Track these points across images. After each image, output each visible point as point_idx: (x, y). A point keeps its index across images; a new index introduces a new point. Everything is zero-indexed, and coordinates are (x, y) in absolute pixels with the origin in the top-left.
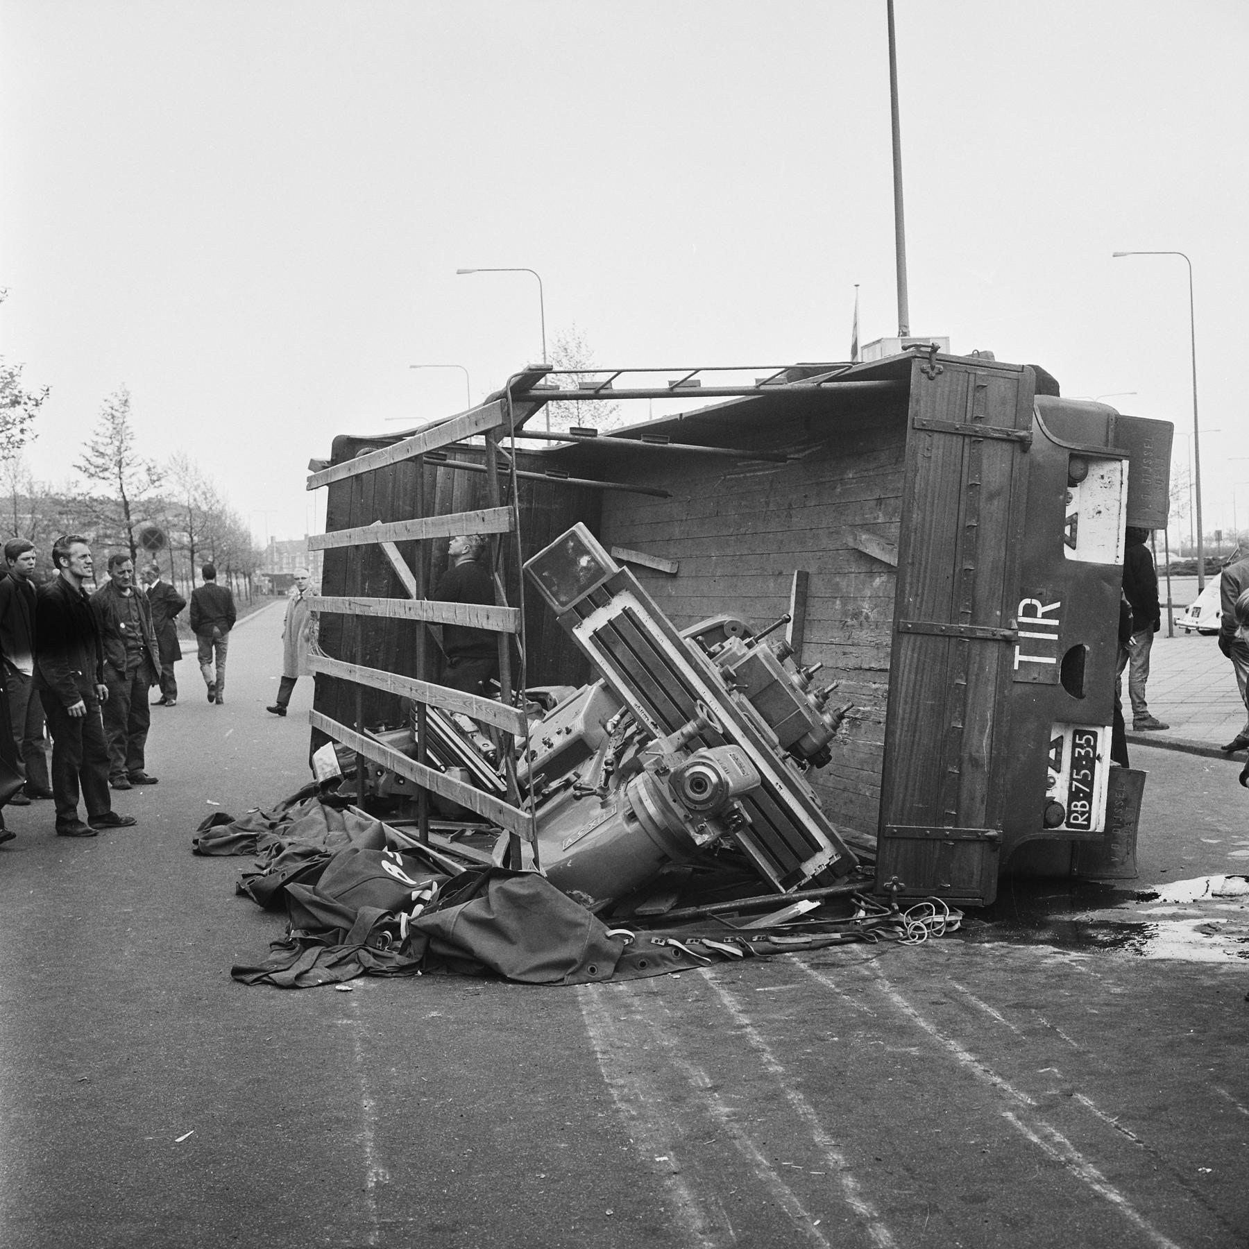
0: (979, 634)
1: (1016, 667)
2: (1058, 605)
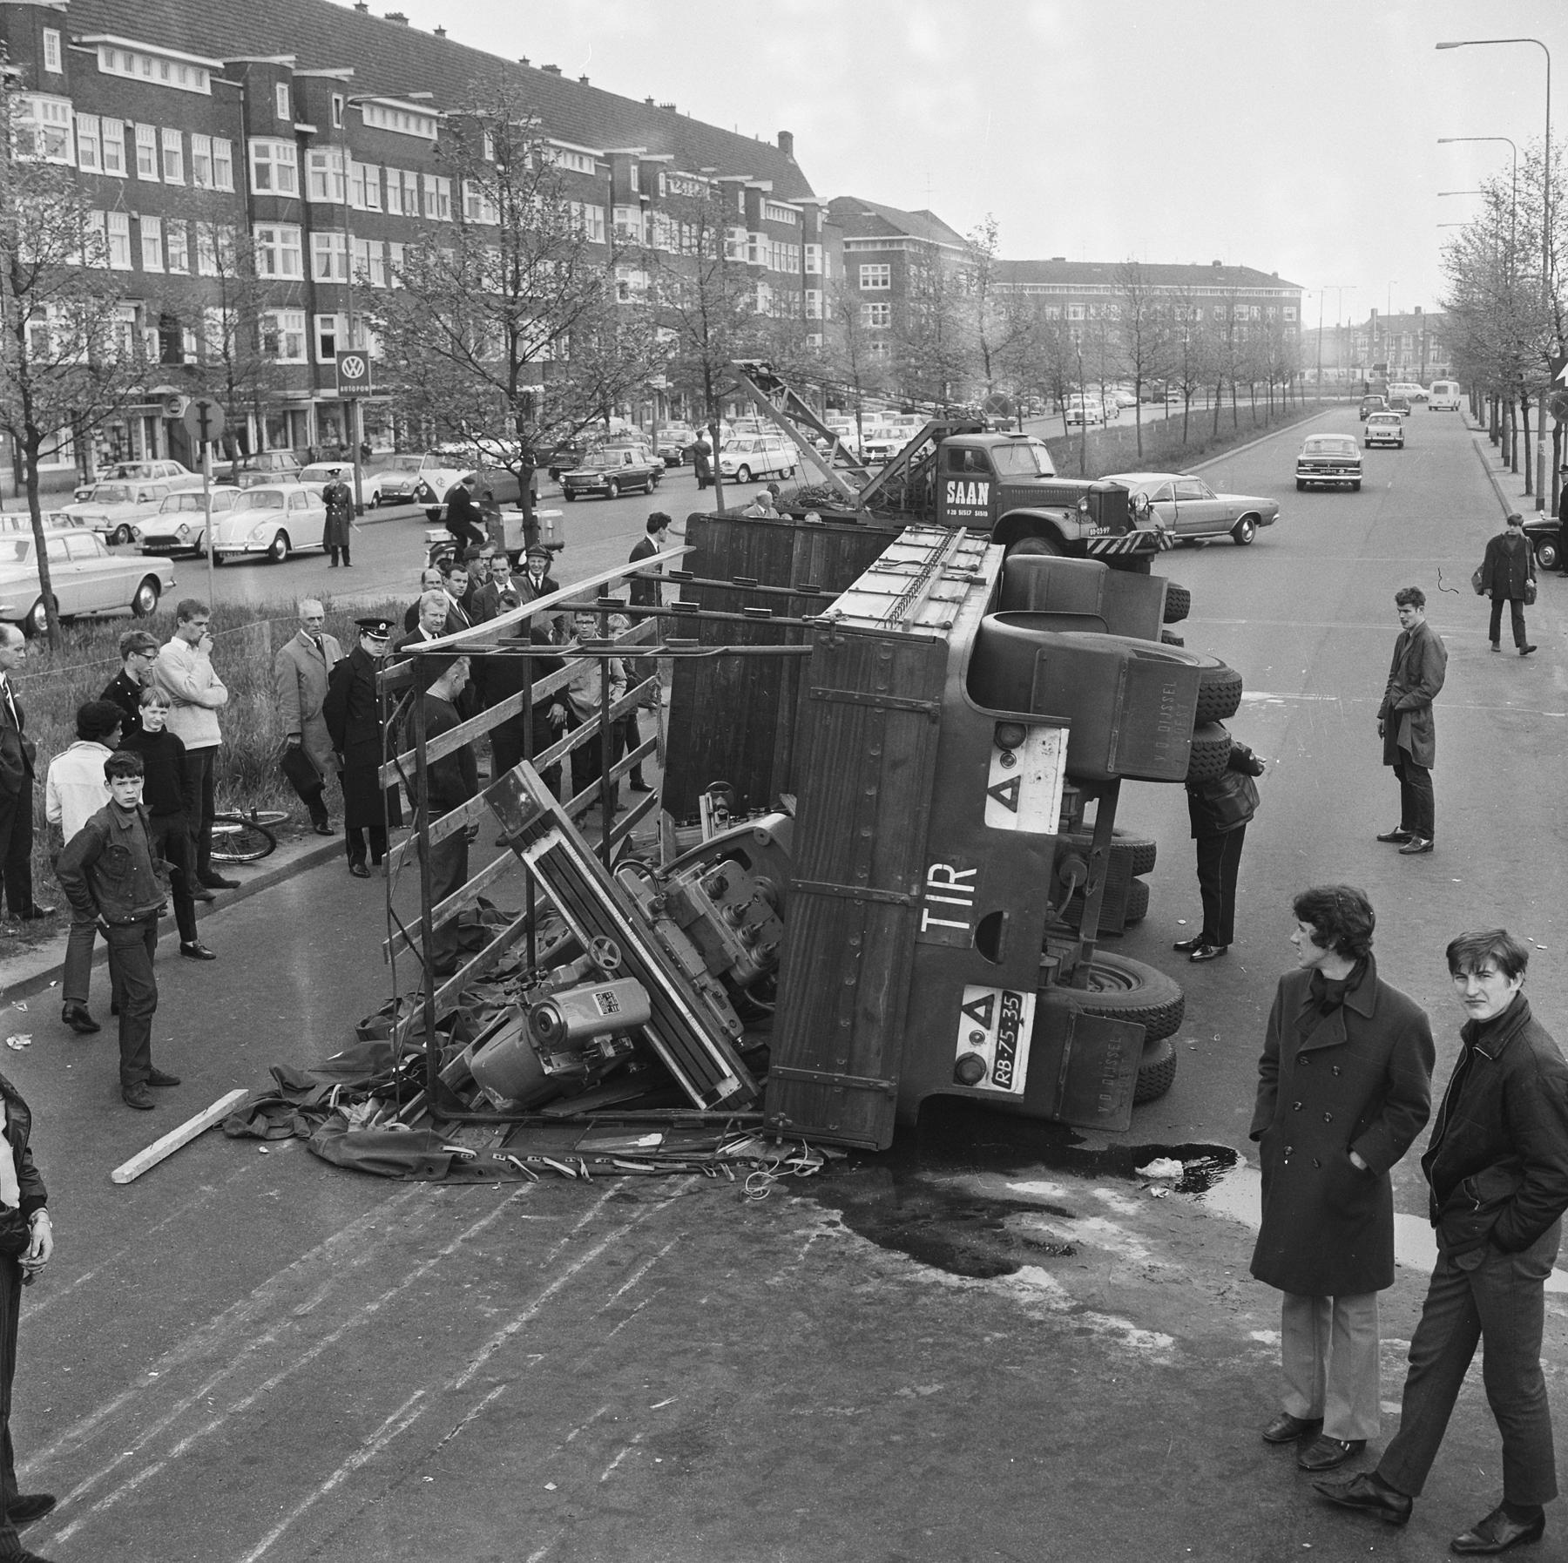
0: (876, 897)
1: (924, 929)
2: (973, 872)
